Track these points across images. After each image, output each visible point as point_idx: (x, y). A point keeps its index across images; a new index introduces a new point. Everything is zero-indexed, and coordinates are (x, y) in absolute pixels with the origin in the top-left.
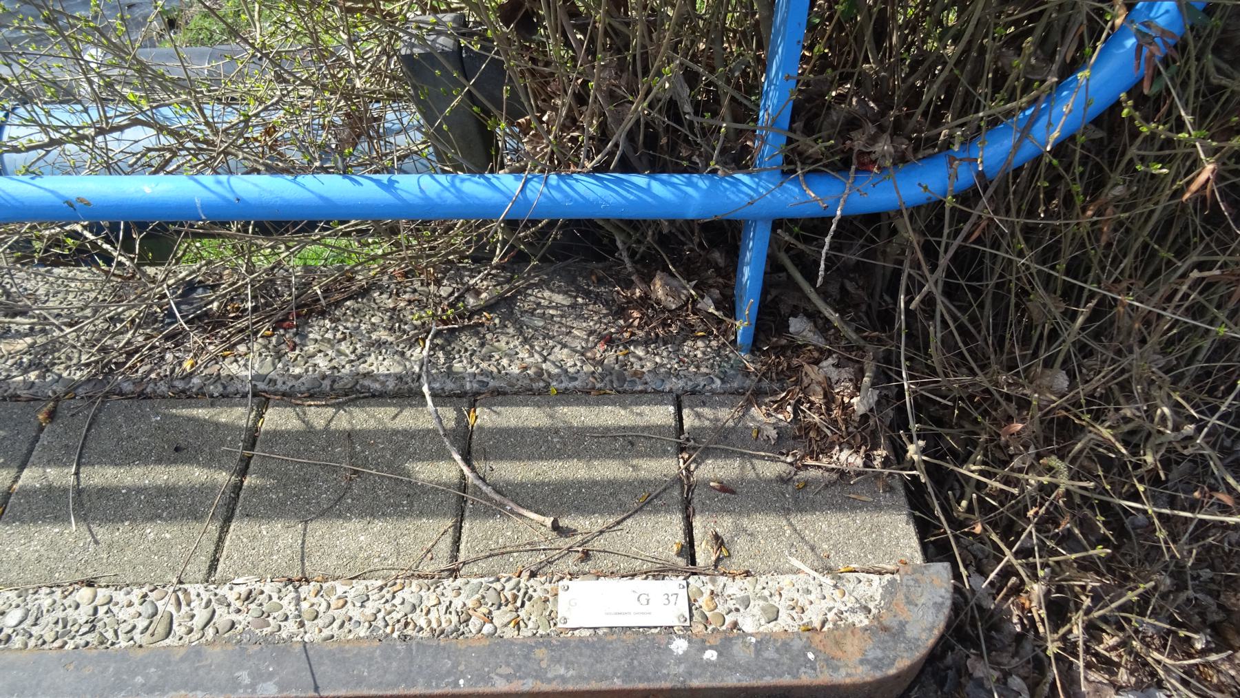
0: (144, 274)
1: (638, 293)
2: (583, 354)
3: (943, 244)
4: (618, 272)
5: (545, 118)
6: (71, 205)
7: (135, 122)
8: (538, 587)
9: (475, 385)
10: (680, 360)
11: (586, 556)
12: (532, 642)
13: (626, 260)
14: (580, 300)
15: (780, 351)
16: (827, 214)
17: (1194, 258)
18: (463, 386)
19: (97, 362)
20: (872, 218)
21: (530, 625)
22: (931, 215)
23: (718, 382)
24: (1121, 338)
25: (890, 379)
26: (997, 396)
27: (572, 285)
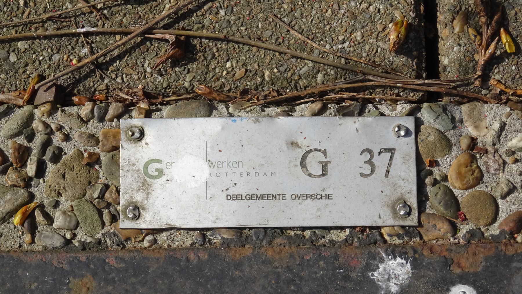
8: (76, 130)
11: (185, 51)
12: (62, 261)
21: (59, 220)
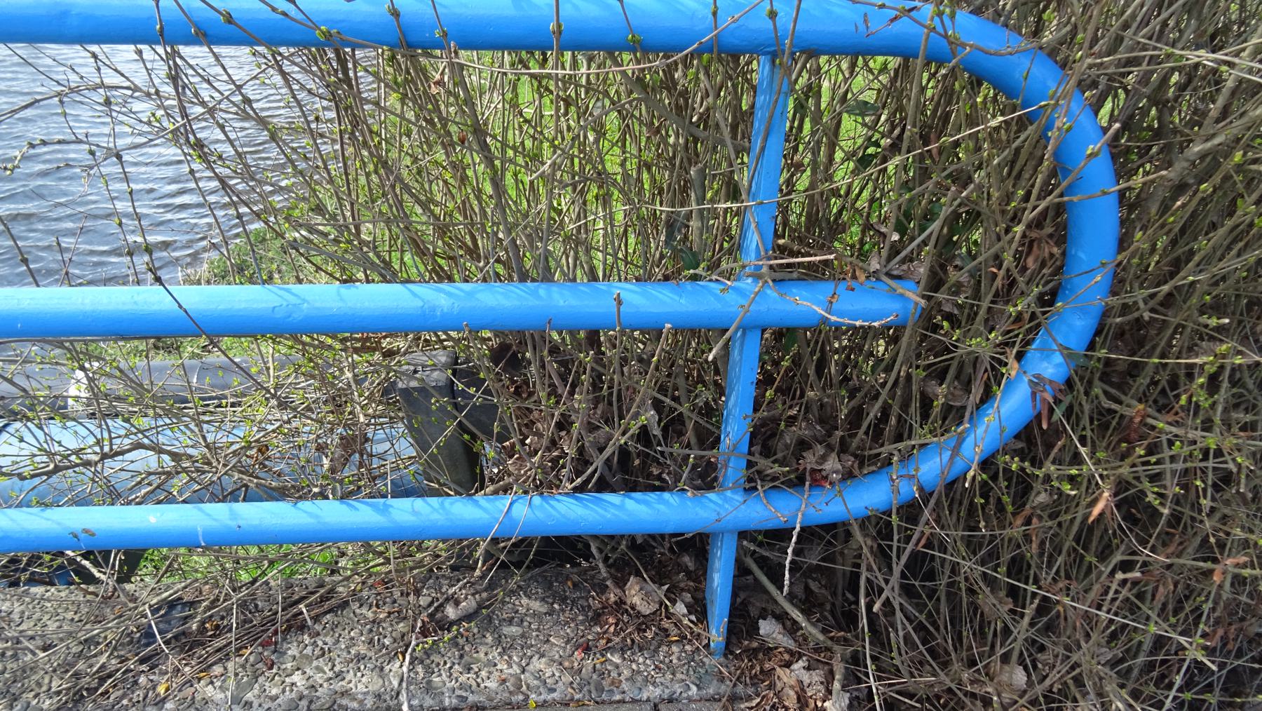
0: (123, 590)
1: (612, 598)
2: (561, 664)
3: (895, 549)
4: (593, 577)
5: (528, 441)
6: (76, 536)
7: (138, 446)
9: (454, 701)
10: (656, 667)
13: (601, 565)
14: (556, 606)
15: (752, 654)
16: (788, 526)
17: (1118, 557)
18: (441, 702)
19: (69, 689)
20: (830, 527)
22: (878, 525)
23: (694, 688)
24: (1068, 633)
25: (859, 681)
26: (960, 694)
27: (553, 595)
